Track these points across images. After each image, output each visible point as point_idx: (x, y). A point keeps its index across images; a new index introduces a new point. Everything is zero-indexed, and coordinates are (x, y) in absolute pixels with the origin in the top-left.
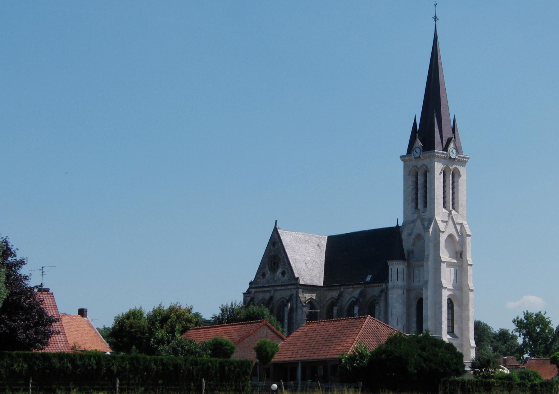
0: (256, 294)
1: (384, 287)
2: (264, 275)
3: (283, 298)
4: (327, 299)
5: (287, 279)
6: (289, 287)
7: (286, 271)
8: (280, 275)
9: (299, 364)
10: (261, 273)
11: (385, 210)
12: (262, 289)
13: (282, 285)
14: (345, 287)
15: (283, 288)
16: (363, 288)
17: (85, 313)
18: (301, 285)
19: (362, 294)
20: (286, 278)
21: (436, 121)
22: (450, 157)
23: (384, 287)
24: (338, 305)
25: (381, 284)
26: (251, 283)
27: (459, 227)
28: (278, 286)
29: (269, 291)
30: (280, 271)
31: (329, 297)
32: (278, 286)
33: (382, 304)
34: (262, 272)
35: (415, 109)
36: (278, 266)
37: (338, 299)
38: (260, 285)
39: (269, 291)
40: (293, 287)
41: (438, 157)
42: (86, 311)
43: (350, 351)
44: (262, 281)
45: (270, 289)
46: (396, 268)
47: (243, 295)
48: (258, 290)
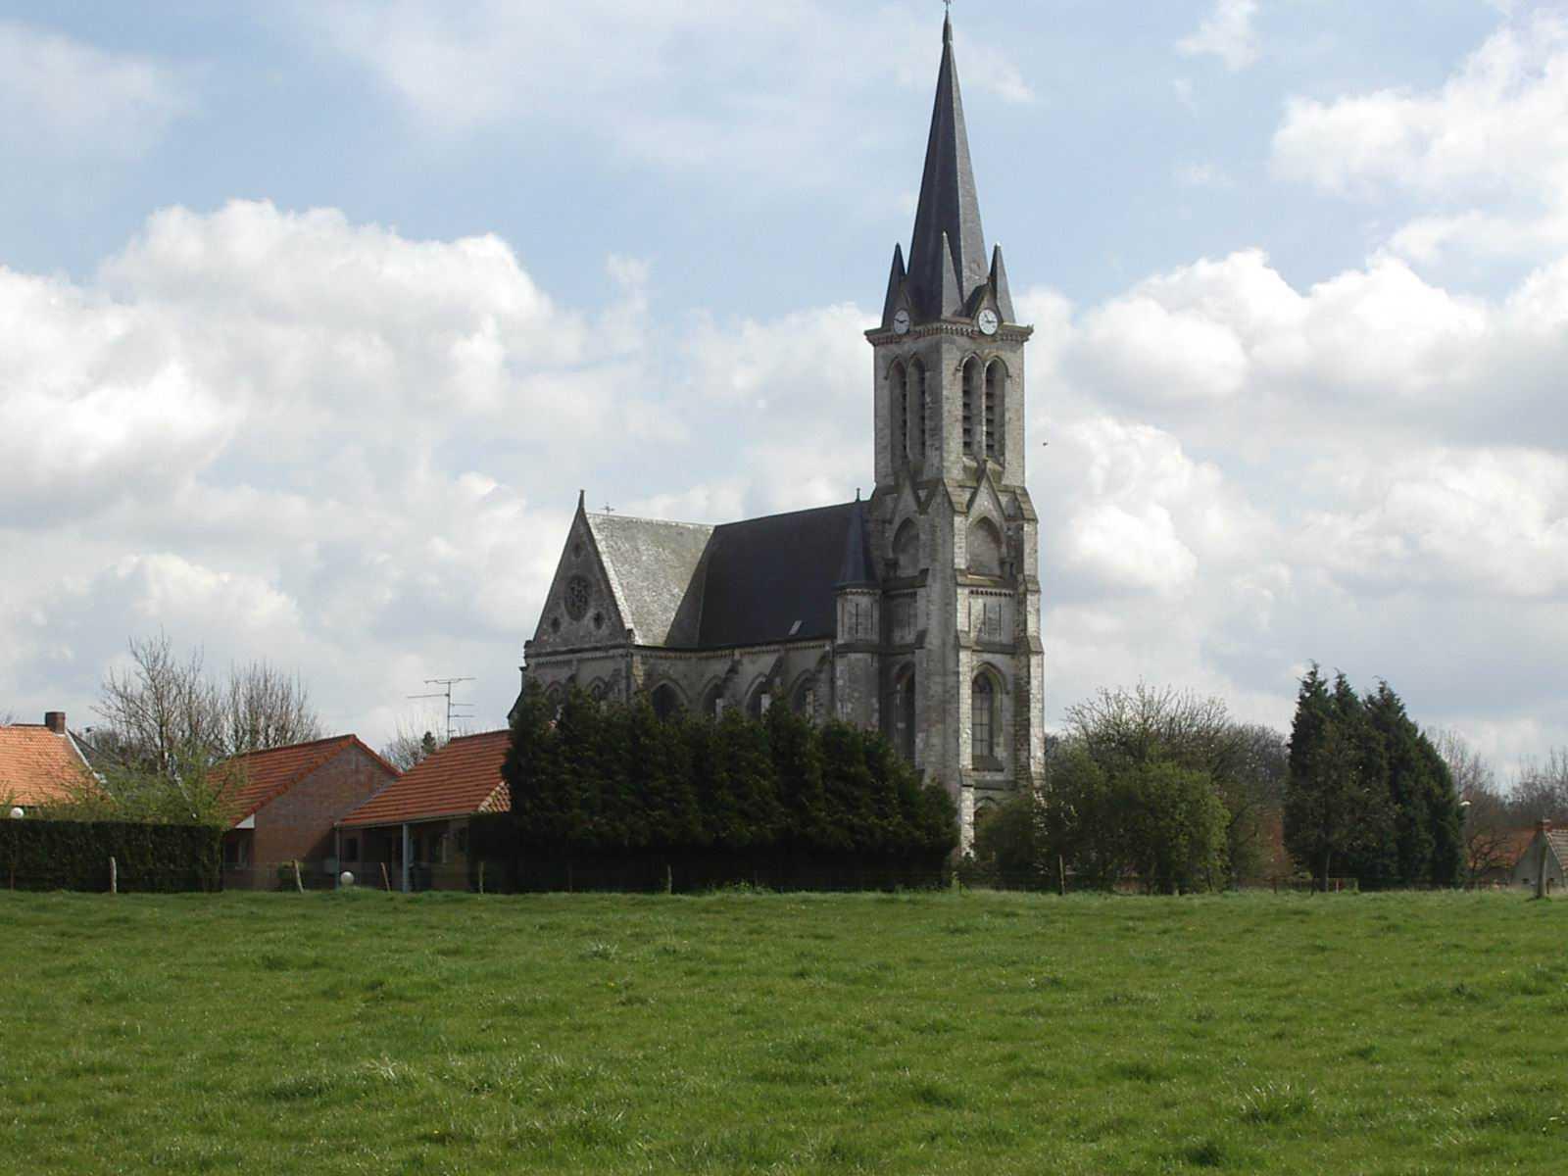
0: (540, 671)
1: (827, 648)
2: (555, 624)
3: (599, 678)
4: (704, 681)
5: (607, 632)
6: (611, 652)
7: (604, 612)
8: (592, 625)
9: (405, 828)
10: (550, 620)
11: (829, 467)
12: (553, 659)
13: (596, 649)
14: (743, 651)
15: (598, 654)
16: (782, 653)
17: (60, 721)
18: (638, 646)
19: (779, 668)
20: (605, 630)
21: (946, 245)
22: (981, 332)
23: (827, 648)
24: (728, 694)
25: (820, 643)
26: (528, 644)
27: (1004, 499)
28: (587, 650)
29: (569, 663)
30: (591, 613)
31: (708, 675)
32: (587, 650)
33: (823, 689)
34: (552, 616)
35: (894, 215)
36: (586, 602)
37: (726, 680)
38: (549, 650)
39: (569, 663)
40: (621, 651)
41: (1001, 321)
42: (64, 718)
43: (485, 804)
44: (553, 640)
45: (570, 656)
46: (856, 609)
47: (520, 672)
48: (542, 660)
